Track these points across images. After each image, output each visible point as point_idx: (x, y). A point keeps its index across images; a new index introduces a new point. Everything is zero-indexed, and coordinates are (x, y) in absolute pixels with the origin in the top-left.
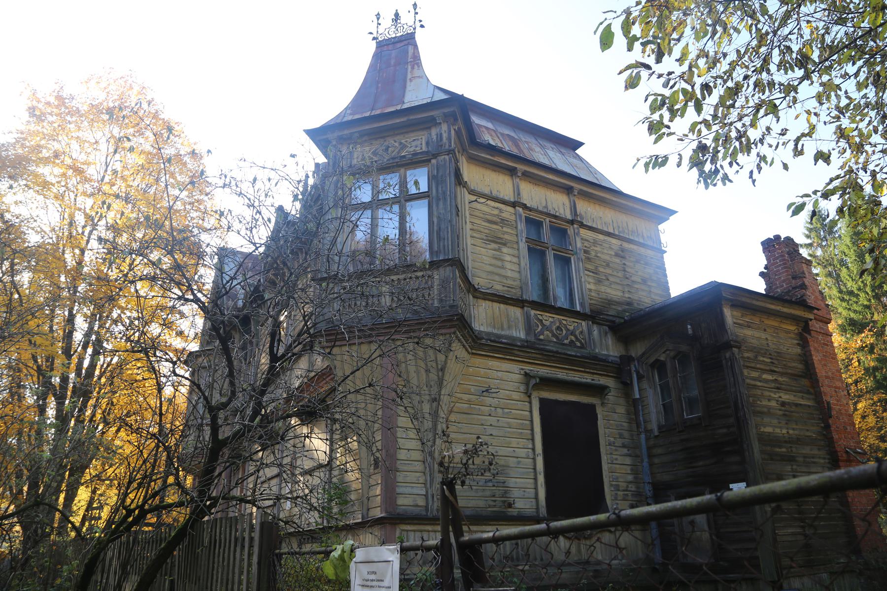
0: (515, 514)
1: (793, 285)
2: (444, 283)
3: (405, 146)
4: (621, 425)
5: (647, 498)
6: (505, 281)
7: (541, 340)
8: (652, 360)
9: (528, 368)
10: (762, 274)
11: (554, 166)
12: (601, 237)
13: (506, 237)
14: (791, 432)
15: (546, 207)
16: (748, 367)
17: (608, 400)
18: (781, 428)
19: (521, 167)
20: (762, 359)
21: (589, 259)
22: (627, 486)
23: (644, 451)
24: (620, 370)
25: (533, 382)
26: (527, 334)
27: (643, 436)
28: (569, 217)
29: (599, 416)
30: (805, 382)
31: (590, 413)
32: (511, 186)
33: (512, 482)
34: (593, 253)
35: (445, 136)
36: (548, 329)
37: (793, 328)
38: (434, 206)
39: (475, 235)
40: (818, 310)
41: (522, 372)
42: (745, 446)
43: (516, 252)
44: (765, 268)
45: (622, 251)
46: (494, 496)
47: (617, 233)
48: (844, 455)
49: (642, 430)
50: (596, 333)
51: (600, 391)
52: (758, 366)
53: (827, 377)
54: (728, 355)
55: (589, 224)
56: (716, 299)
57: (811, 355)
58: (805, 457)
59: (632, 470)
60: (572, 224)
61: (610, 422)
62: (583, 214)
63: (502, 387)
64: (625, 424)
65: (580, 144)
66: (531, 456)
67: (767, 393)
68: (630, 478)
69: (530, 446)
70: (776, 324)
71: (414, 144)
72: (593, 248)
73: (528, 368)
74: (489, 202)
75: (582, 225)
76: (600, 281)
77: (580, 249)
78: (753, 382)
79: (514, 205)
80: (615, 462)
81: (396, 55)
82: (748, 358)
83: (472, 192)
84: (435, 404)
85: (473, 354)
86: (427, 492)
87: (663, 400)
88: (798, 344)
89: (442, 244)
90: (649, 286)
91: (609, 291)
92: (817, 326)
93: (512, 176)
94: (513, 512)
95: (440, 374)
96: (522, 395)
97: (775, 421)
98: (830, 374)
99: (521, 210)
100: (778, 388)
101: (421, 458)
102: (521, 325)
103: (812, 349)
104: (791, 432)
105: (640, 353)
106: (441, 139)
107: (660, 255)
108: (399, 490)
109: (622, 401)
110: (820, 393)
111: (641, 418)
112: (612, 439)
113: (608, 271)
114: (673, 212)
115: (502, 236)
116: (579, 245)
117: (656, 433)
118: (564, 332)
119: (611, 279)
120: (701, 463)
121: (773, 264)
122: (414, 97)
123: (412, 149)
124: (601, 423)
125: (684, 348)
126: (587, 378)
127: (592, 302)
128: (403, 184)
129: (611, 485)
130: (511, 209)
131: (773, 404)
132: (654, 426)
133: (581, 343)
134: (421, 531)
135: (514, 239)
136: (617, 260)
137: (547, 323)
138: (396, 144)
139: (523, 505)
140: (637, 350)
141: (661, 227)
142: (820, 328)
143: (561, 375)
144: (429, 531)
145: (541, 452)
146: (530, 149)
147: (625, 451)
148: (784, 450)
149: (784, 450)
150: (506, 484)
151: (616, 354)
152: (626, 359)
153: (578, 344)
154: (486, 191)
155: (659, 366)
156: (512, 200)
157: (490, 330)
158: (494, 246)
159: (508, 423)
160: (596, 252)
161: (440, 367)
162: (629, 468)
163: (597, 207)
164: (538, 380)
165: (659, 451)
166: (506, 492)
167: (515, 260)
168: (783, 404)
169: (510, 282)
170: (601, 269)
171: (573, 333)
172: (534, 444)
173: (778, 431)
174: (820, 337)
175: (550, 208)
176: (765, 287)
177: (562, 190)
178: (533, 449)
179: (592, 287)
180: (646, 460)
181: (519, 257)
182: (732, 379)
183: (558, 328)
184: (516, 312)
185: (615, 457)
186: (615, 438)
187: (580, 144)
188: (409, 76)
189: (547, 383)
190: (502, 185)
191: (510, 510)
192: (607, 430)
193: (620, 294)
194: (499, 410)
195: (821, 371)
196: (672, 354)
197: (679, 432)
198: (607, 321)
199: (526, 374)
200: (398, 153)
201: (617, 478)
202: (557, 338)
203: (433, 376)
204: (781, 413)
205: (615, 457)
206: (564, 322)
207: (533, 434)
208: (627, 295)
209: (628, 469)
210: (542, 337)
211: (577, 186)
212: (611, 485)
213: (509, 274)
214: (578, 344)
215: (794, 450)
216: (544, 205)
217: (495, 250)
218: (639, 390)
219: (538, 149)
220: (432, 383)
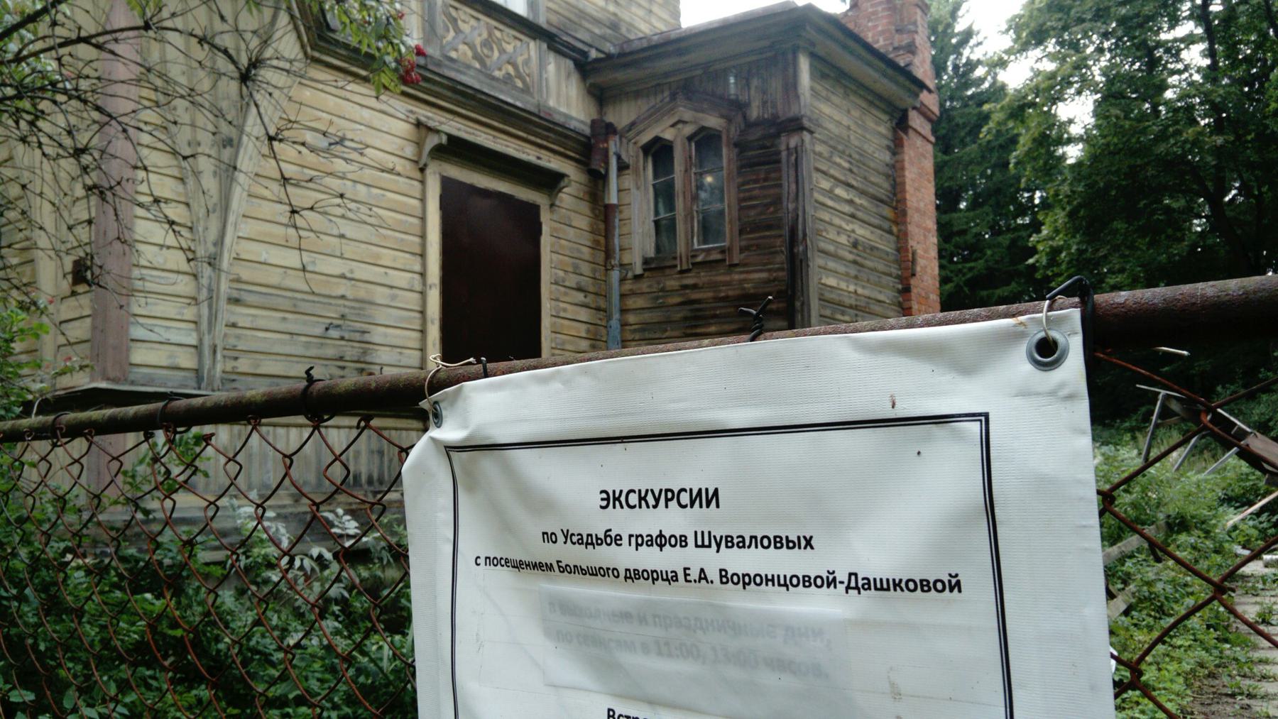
1: (896, 45)
4: (579, 251)
7: (451, 60)
8: (646, 138)
9: (424, 113)
16: (818, 170)
20: (838, 160)
24: (588, 149)
25: (432, 141)
29: (545, 229)
30: (887, 212)
31: (528, 220)
33: (377, 335)
42: (798, 304)
46: (341, 359)
50: (551, 68)
51: (549, 182)
52: (832, 172)
53: (918, 210)
54: (793, 142)
57: (903, 169)
59: (588, 331)
63: (369, 141)
66: (418, 287)
69: (418, 268)
78: (821, 198)
80: (562, 314)
86: (201, 340)
88: (888, 148)
98: (922, 205)
100: (853, 216)
103: (906, 158)
109: (585, 207)
110: (906, 234)
111: (616, 241)
112: (561, 274)
117: (639, 271)
118: (496, 54)
124: (546, 241)
126: (528, 154)
131: (843, 239)
133: (524, 82)
147: (580, 297)
150: (367, 337)
151: (582, 117)
152: (604, 130)
153: (519, 84)
155: (659, 152)
164: (444, 139)
165: (639, 302)
168: (855, 245)
172: (424, 265)
178: (423, 275)
180: (616, 316)
182: (793, 186)
185: (562, 305)
189: (455, 149)
192: (555, 256)
196: (688, 130)
198: (574, 49)
199: (418, 124)
201: (563, 343)
206: (498, 34)
207: (424, 245)
209: (582, 330)
210: (453, 55)
214: (519, 84)
218: (619, 191)
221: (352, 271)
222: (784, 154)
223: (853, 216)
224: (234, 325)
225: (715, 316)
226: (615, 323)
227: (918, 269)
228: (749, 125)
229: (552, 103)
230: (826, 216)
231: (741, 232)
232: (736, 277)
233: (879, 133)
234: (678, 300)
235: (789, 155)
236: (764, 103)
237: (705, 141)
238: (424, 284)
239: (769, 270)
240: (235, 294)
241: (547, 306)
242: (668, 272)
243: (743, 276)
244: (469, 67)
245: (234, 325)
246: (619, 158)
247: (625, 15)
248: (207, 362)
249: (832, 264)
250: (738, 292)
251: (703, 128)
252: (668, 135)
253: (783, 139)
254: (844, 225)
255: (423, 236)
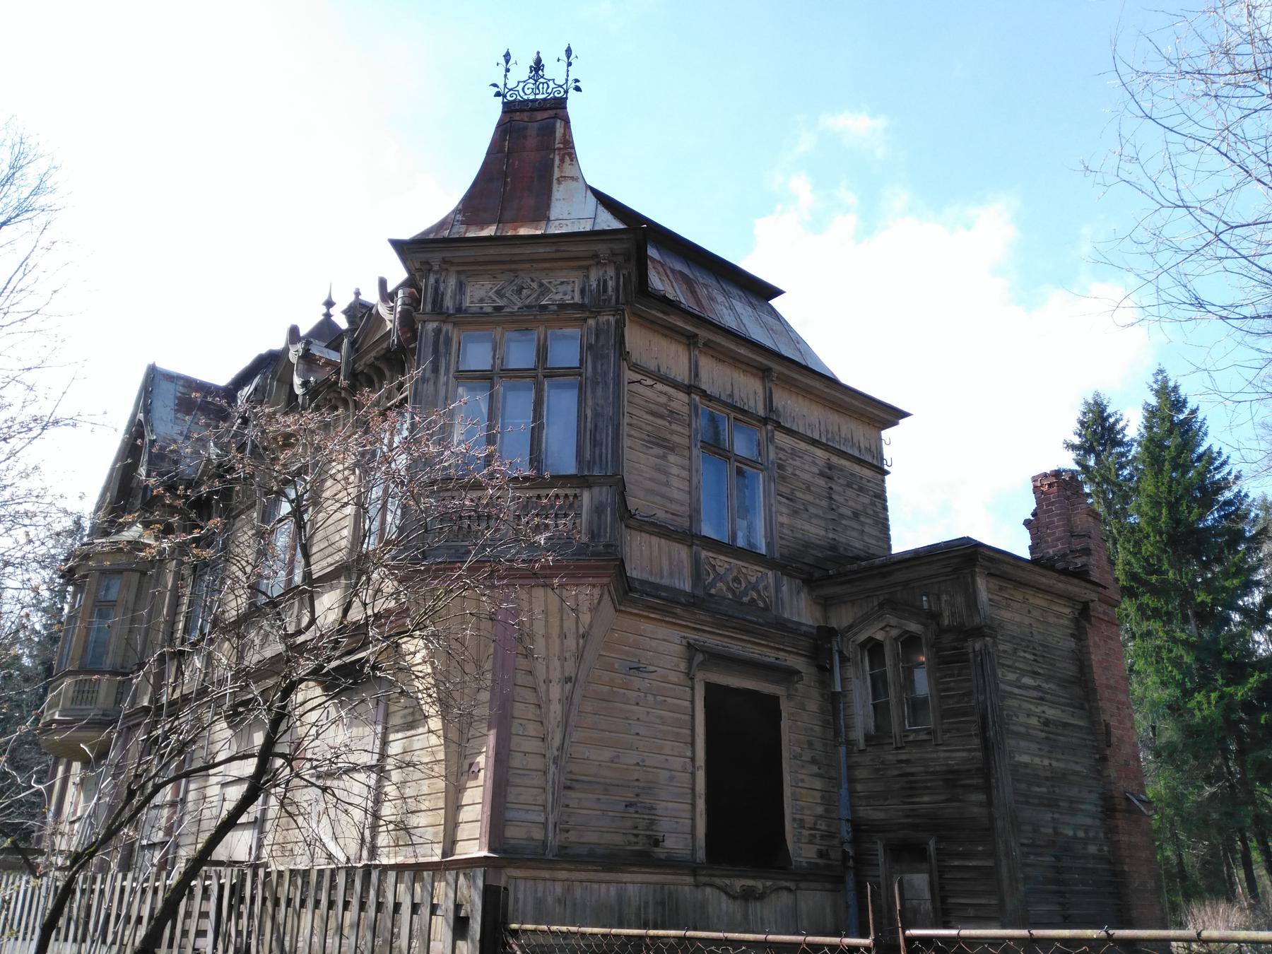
0: (663, 856)
2: (598, 510)
3: (547, 291)
4: (812, 729)
5: (842, 843)
6: (669, 505)
8: (862, 637)
9: (692, 636)
10: (1027, 523)
11: (742, 331)
12: (803, 445)
13: (676, 438)
14: (1055, 764)
15: (731, 396)
17: (796, 690)
18: (1041, 757)
19: (703, 334)
20: (1022, 654)
21: (783, 478)
22: (815, 824)
23: (844, 770)
24: (821, 646)
26: (694, 585)
27: (843, 749)
28: (761, 412)
29: (784, 714)
31: (770, 707)
32: (686, 361)
34: (790, 470)
35: (611, 284)
36: (719, 578)
37: (1067, 611)
38: (589, 394)
39: (632, 432)
40: (1105, 588)
41: (684, 642)
43: (687, 462)
44: (1033, 515)
45: (830, 469)
46: (636, 828)
47: (824, 440)
48: (1124, 803)
49: (842, 739)
51: (787, 675)
52: (1017, 664)
53: (1108, 687)
55: (788, 425)
56: (965, 556)
57: (1089, 653)
58: (1071, 802)
59: (822, 798)
60: (766, 424)
61: (798, 726)
62: (781, 409)
64: (817, 729)
65: (776, 292)
67: (1026, 705)
68: (820, 810)
69: (689, 754)
70: (1044, 603)
71: (561, 288)
72: (790, 461)
73: (692, 636)
74: (659, 386)
75: (779, 426)
76: (795, 512)
77: (773, 463)
79: (689, 389)
81: (532, 136)
82: (1005, 652)
83: (635, 368)
84: (569, 686)
85: (620, 611)
87: (874, 698)
88: (1072, 635)
89: (597, 452)
90: (863, 524)
91: (807, 527)
92: (1100, 609)
93: (689, 345)
94: (660, 852)
95: (581, 641)
96: (682, 677)
97: (1034, 747)
99: (697, 398)
100: (1041, 699)
101: (541, 767)
102: (687, 572)
104: (1055, 764)
105: (845, 624)
106: (605, 290)
107: (880, 477)
108: (509, 815)
112: (799, 750)
113: (809, 498)
114: (904, 415)
115: (669, 436)
116: (772, 456)
117: (862, 746)
119: (812, 510)
120: (926, 799)
121: (1046, 512)
122: (570, 214)
123: (558, 297)
124: (785, 724)
125: (914, 627)
126: (769, 656)
127: (784, 542)
128: (542, 353)
129: (794, 820)
130: (683, 396)
131: (1034, 721)
132: (858, 735)
133: (765, 602)
134: (535, 879)
135: (685, 442)
136: (822, 482)
137: (721, 571)
138: (535, 285)
139: (674, 844)
140: (842, 618)
141: (886, 434)
142: (1105, 613)
143: (736, 648)
144: (545, 879)
145: (703, 764)
146: (712, 299)
147: (815, 769)
148: (1044, 790)
149: (1044, 790)
151: (810, 622)
154: (652, 366)
155: (874, 649)
156: (686, 382)
157: (646, 576)
158: (657, 451)
159: (661, 718)
160: (795, 468)
161: (581, 631)
162: (818, 794)
163: (800, 399)
166: (652, 822)
167: (685, 474)
168: (1047, 722)
169: (675, 507)
170: (799, 494)
171: (755, 588)
172: (693, 752)
173: (1037, 761)
174: (1104, 627)
175: (736, 397)
176: (1028, 542)
177: (755, 371)
178: (693, 759)
179: (785, 520)
180: (845, 786)
181: (690, 471)
183: (736, 580)
184: (682, 553)
186: (802, 749)
187: (776, 292)
188: (557, 174)
190: (672, 358)
191: (656, 850)
193: (822, 533)
194: (650, 698)
195: (1100, 676)
196: (895, 633)
197: (897, 748)
199: (689, 646)
200: (537, 299)
201: (802, 809)
202: (734, 593)
203: (571, 643)
204: (1043, 735)
205: (801, 777)
206: (744, 570)
208: (831, 535)
210: (713, 591)
211: (777, 367)
212: (794, 820)
213: (676, 494)
214: (761, 604)
215: (1057, 790)
216: (729, 392)
217: (658, 457)
219: (720, 298)
220: (567, 655)
221: (643, 761)
222: (971, 656)
223: (1041, 699)
224: (567, 806)
225: (927, 788)
226: (844, 791)
227: (1114, 740)
228: (942, 631)
229: (786, 615)
230: (1015, 703)
231: (943, 717)
232: (942, 755)
233: (1062, 625)
234: (896, 772)
235: (976, 656)
236: (953, 614)
237: (910, 643)
238: (694, 766)
239: (969, 751)
240: (568, 783)
241: (787, 791)
242: (886, 747)
243: (947, 754)
244: (724, 598)
245: (567, 806)
246: (841, 653)
247: (842, 539)
248: (551, 835)
249: (1023, 744)
250: (944, 768)
251: (906, 632)
252: (879, 636)
253: (970, 643)
254: (1033, 708)
255: (693, 730)
